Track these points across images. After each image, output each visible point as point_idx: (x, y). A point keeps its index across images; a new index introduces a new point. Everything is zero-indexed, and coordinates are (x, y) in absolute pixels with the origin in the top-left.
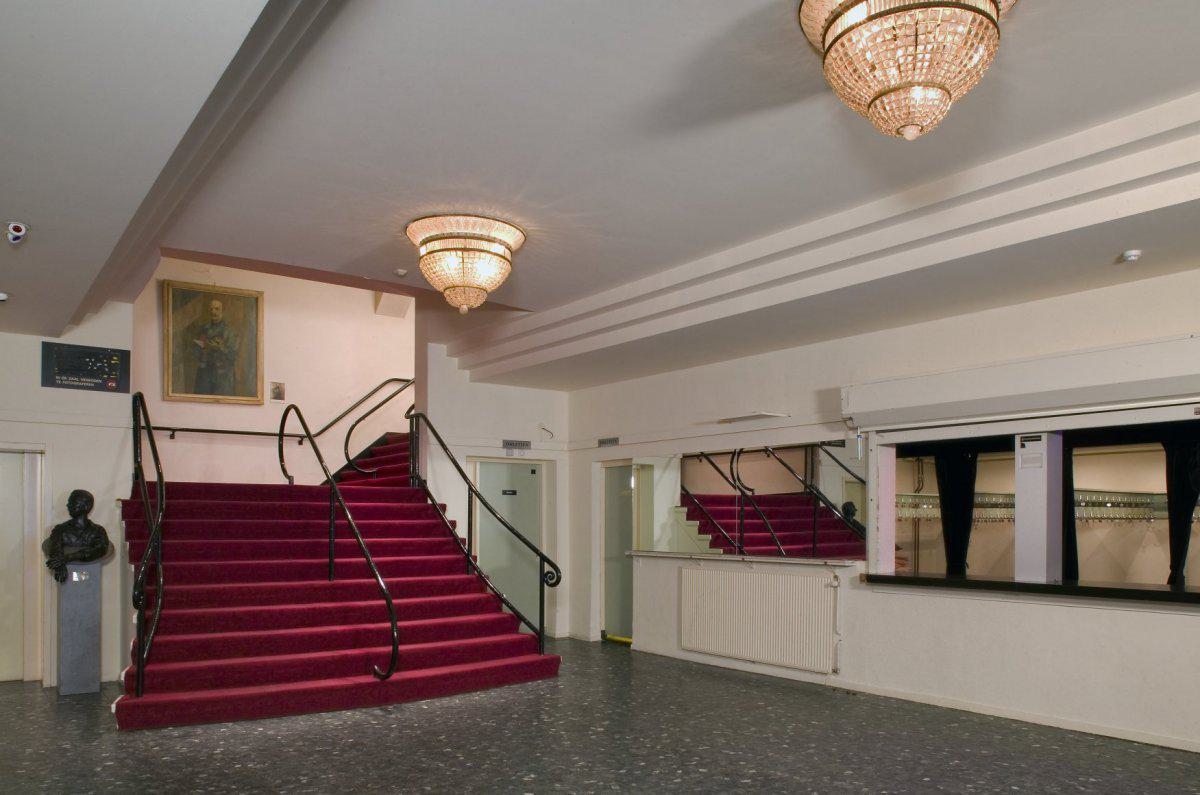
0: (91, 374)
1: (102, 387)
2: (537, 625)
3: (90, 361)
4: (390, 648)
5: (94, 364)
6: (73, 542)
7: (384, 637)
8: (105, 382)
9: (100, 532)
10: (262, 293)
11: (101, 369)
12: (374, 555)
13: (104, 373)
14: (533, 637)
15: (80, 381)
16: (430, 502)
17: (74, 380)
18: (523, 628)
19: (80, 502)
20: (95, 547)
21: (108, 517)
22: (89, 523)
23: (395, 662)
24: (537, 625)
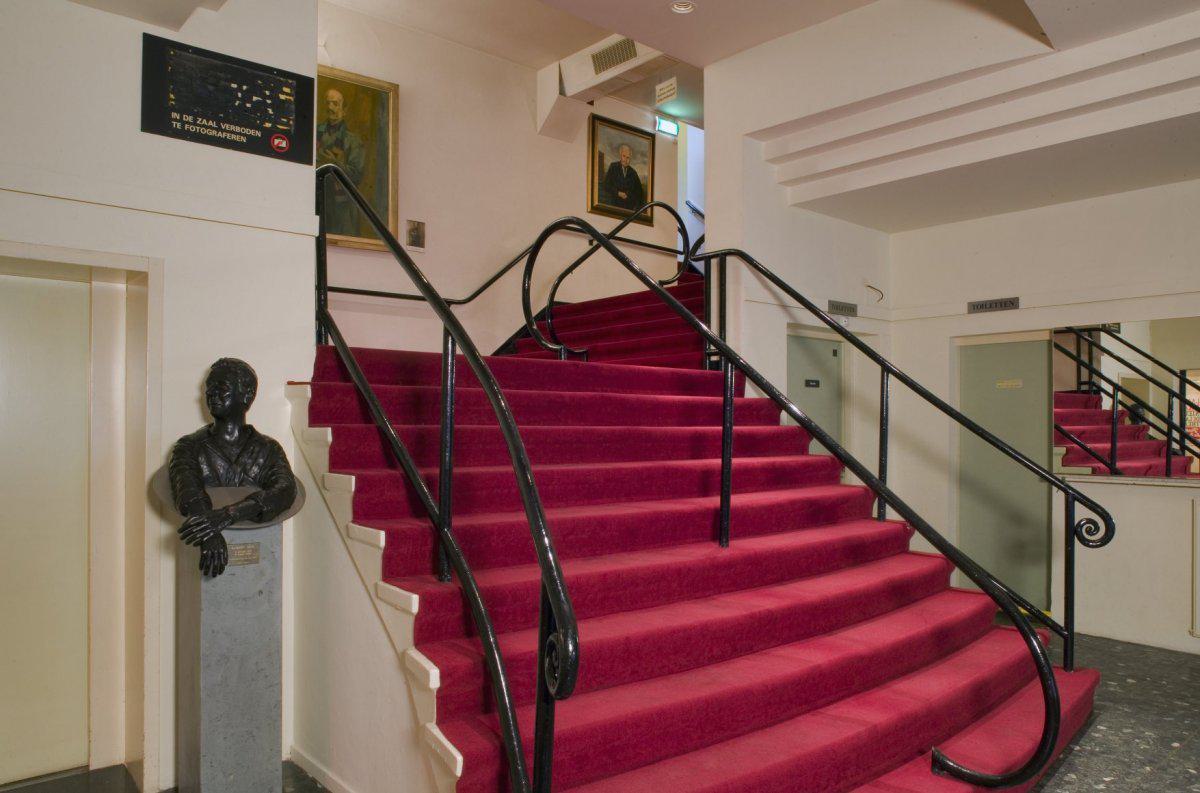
0: (242, 118)
1: (259, 147)
2: (874, 471)
3: (239, 89)
4: (718, 461)
5: (247, 97)
6: (216, 485)
7: (703, 483)
8: (269, 135)
9: (273, 450)
10: (652, 226)
11: (260, 107)
12: (535, 460)
13: (266, 117)
14: (866, 489)
15: (219, 129)
16: (892, 514)
17: (207, 126)
18: (851, 479)
19: (229, 385)
20: (275, 494)
21: (279, 414)
22: (249, 432)
23: (725, 482)
24: (874, 471)
